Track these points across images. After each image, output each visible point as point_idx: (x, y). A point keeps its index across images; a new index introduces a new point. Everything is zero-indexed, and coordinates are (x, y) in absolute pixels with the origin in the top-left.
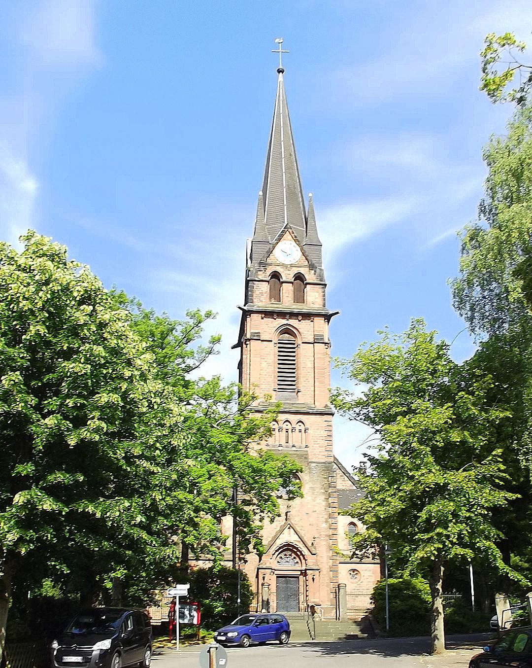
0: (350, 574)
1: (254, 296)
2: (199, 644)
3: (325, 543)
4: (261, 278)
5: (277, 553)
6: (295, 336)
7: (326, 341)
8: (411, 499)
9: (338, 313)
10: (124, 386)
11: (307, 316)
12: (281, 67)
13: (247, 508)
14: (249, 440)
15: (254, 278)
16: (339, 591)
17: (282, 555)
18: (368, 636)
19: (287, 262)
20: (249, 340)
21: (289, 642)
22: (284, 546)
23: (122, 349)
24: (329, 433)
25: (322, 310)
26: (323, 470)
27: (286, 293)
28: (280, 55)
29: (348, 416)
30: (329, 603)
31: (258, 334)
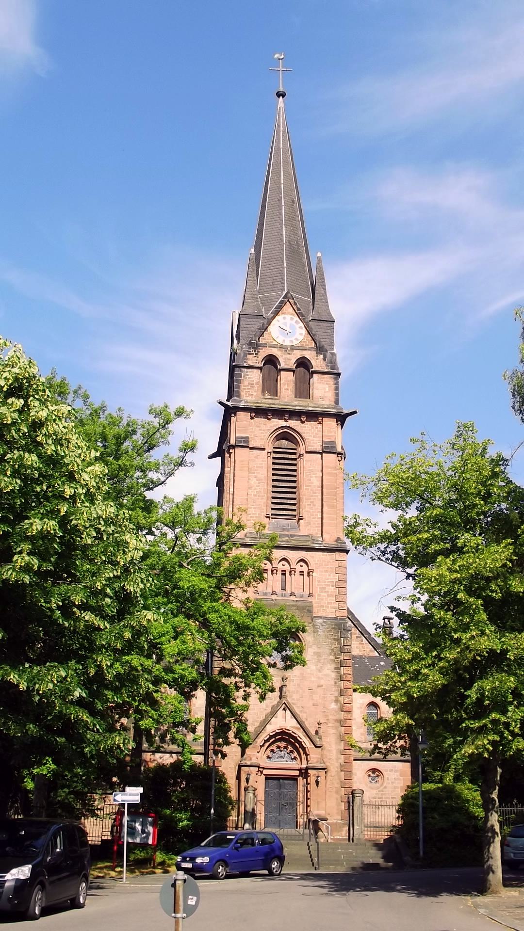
0: (369, 775)
1: (242, 387)
3: (333, 731)
6: (296, 442)
7: (339, 450)
8: (456, 671)
9: (355, 412)
11: (314, 416)
12: (281, 89)
13: (226, 681)
14: (232, 586)
15: (240, 363)
17: (274, 747)
19: (287, 343)
20: (234, 447)
21: (282, 872)
23: (63, 457)
26: (333, 628)
27: (285, 384)
29: (369, 555)
30: (340, 818)
31: (246, 439)
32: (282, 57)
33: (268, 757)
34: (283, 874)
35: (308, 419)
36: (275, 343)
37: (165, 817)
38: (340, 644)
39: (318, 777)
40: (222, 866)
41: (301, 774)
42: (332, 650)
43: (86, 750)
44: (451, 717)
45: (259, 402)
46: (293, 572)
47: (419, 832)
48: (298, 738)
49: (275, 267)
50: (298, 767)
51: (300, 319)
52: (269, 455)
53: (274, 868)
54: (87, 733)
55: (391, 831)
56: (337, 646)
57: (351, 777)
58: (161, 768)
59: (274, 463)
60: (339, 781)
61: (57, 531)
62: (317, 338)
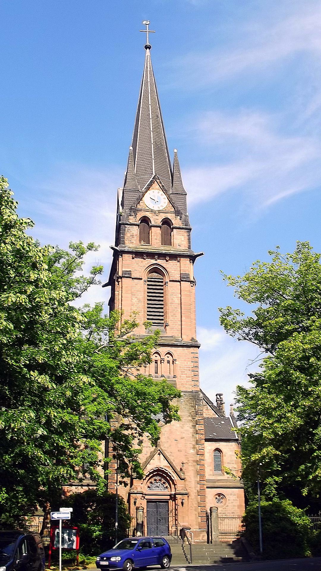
0: (216, 498)
1: (126, 238)
2: (78, 569)
3: (193, 468)
4: (131, 221)
5: (148, 478)
6: (163, 275)
7: (192, 279)
8: (307, 416)
9: (202, 254)
10: (30, 289)
11: (174, 257)
12: (148, 44)
13: (126, 432)
14: (129, 366)
15: (125, 222)
16: (211, 515)
17: (152, 480)
18: (242, 559)
19: (156, 208)
20: (121, 278)
21: (170, 566)
22: (155, 471)
23: (28, 252)
24: (196, 364)
25: (187, 252)
26: (190, 399)
27: (154, 236)
28: (148, 29)
29: (237, 335)
30: (198, 527)
31: (129, 272)
32: (148, 23)
33: (149, 487)
34: (171, 567)
35: (170, 259)
36: (147, 208)
37: (83, 529)
38: (195, 409)
39: (183, 500)
40: (130, 563)
41: (171, 498)
42: (190, 413)
43: (39, 479)
44: (305, 449)
45: (138, 247)
46: (162, 361)
47: (259, 535)
48: (169, 473)
49: (146, 159)
50: (169, 493)
51: (164, 193)
52: (145, 283)
53: (165, 563)
54: (39, 466)
55: (237, 535)
56: (193, 410)
57: (205, 499)
58: (78, 495)
59: (148, 288)
60: (197, 502)
61: (27, 303)
62: (175, 205)
